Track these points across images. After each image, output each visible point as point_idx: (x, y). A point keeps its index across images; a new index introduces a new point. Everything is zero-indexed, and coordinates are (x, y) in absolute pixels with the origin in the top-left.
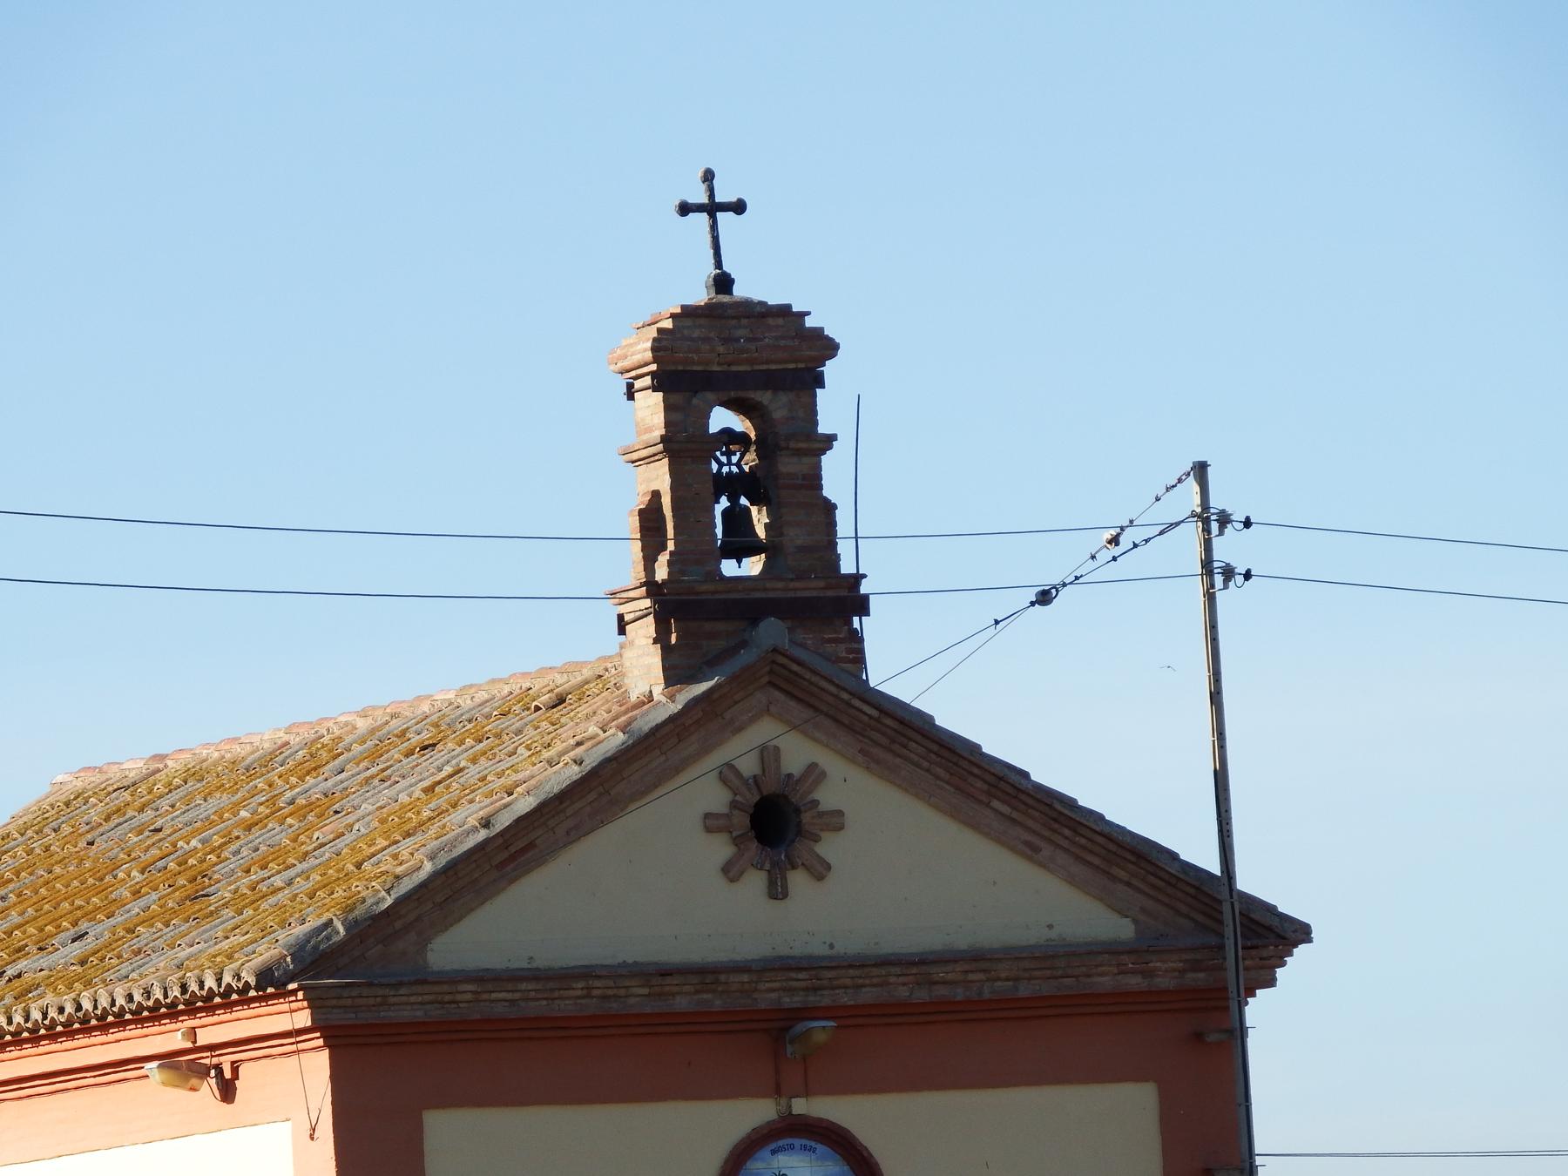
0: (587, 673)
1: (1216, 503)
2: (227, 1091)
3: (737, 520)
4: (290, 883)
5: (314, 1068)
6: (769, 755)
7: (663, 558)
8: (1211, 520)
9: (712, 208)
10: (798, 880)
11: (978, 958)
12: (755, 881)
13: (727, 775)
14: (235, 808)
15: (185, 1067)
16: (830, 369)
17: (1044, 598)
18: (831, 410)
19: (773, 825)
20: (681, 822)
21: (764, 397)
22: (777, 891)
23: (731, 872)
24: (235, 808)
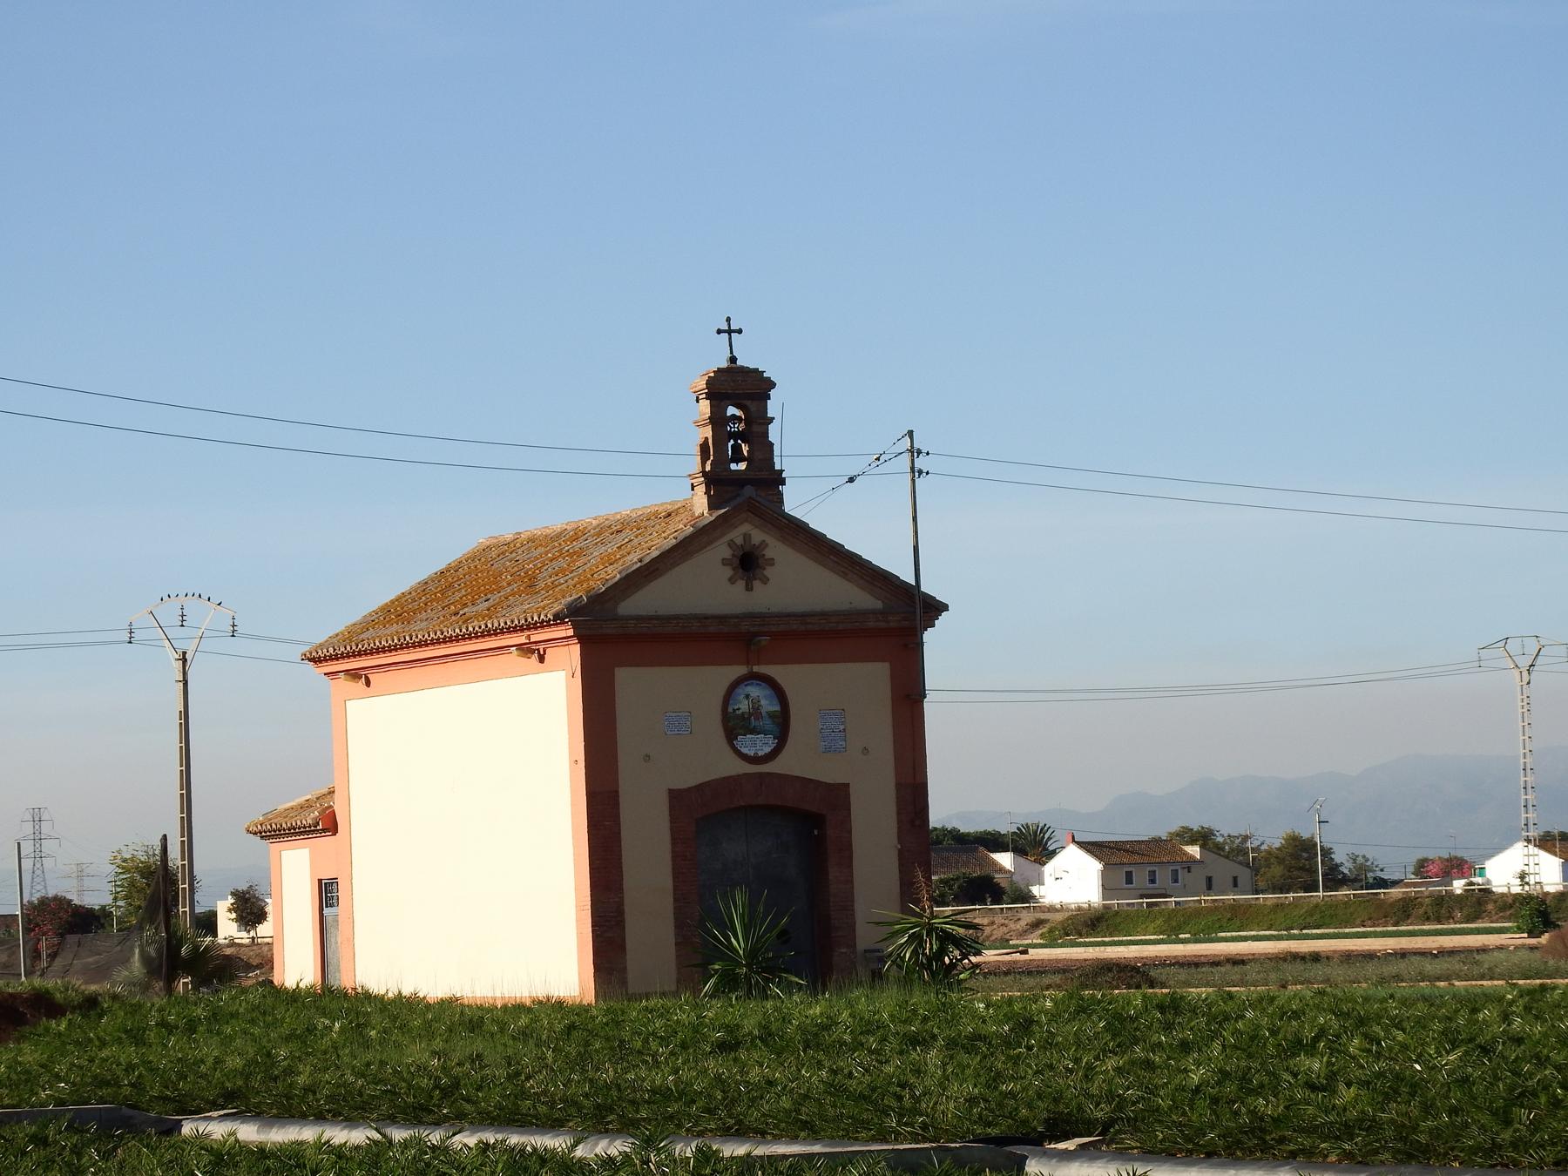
1: (916, 446)
2: (542, 659)
6: (747, 537)
8: (914, 452)
9: (730, 332)
10: (756, 584)
12: (741, 584)
13: (731, 544)
15: (526, 650)
16: (772, 392)
17: (851, 480)
18: (773, 408)
19: (748, 563)
21: (748, 403)
22: (749, 588)
23: (732, 580)
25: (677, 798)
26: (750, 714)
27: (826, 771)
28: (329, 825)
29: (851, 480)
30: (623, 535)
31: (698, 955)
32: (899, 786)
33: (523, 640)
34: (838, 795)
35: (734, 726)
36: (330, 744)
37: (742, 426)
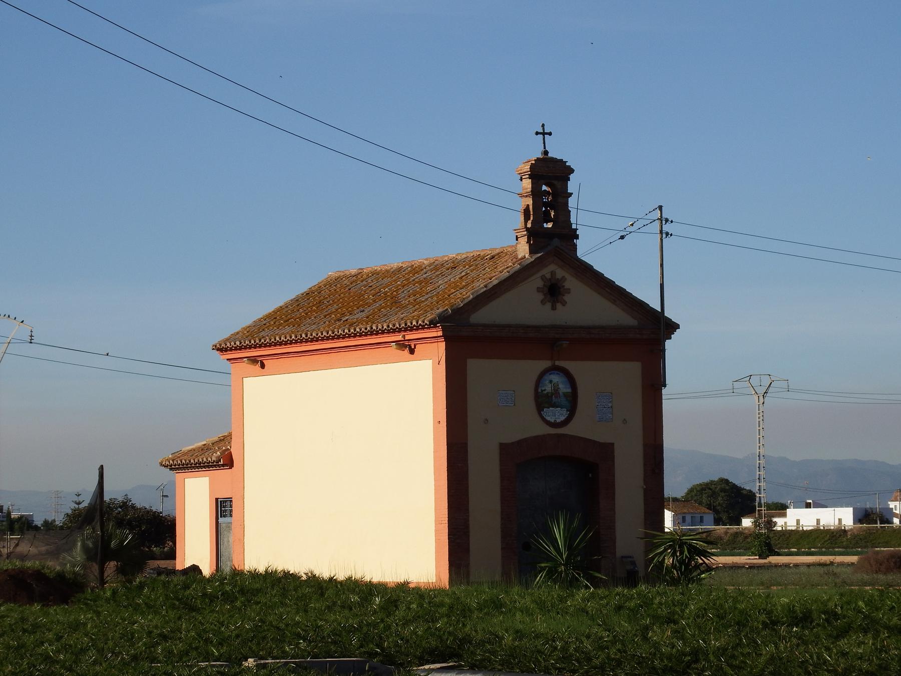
0: (497, 251)
2: (412, 351)
3: (547, 213)
4: (426, 300)
5: (441, 347)
6: (553, 273)
7: (530, 222)
8: (663, 220)
9: (544, 134)
10: (559, 306)
11: (602, 328)
12: (559, 306)
13: (543, 278)
14: (395, 281)
15: (401, 345)
16: (571, 176)
17: (622, 237)
18: (572, 186)
19: (554, 292)
20: (531, 289)
21: (555, 182)
22: (554, 308)
24: (395, 281)
25: (505, 449)
26: (552, 394)
27: (600, 435)
28: (228, 462)
29: (622, 237)
30: (455, 272)
31: (523, 555)
32: (645, 446)
33: (400, 338)
34: (607, 450)
35: (543, 401)
36: (231, 408)
37: (550, 198)
